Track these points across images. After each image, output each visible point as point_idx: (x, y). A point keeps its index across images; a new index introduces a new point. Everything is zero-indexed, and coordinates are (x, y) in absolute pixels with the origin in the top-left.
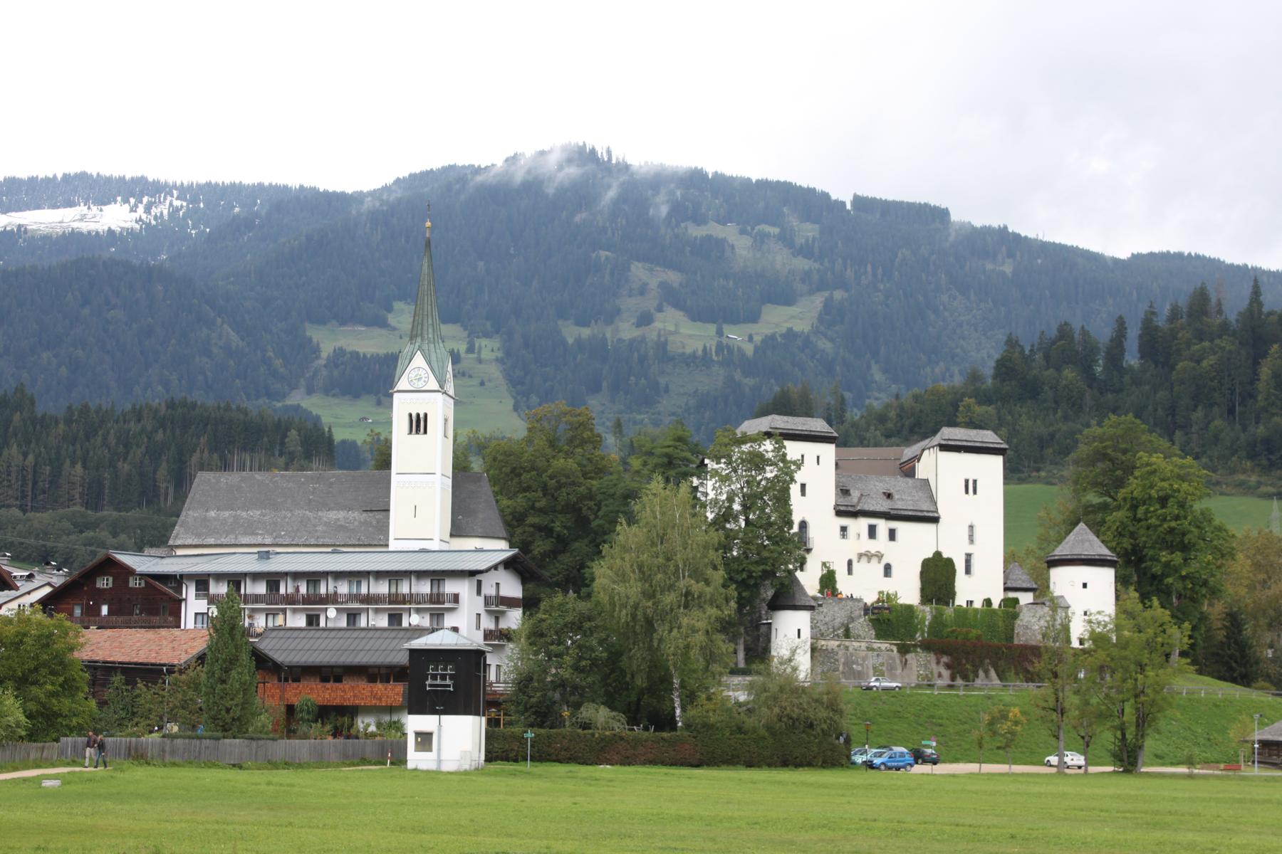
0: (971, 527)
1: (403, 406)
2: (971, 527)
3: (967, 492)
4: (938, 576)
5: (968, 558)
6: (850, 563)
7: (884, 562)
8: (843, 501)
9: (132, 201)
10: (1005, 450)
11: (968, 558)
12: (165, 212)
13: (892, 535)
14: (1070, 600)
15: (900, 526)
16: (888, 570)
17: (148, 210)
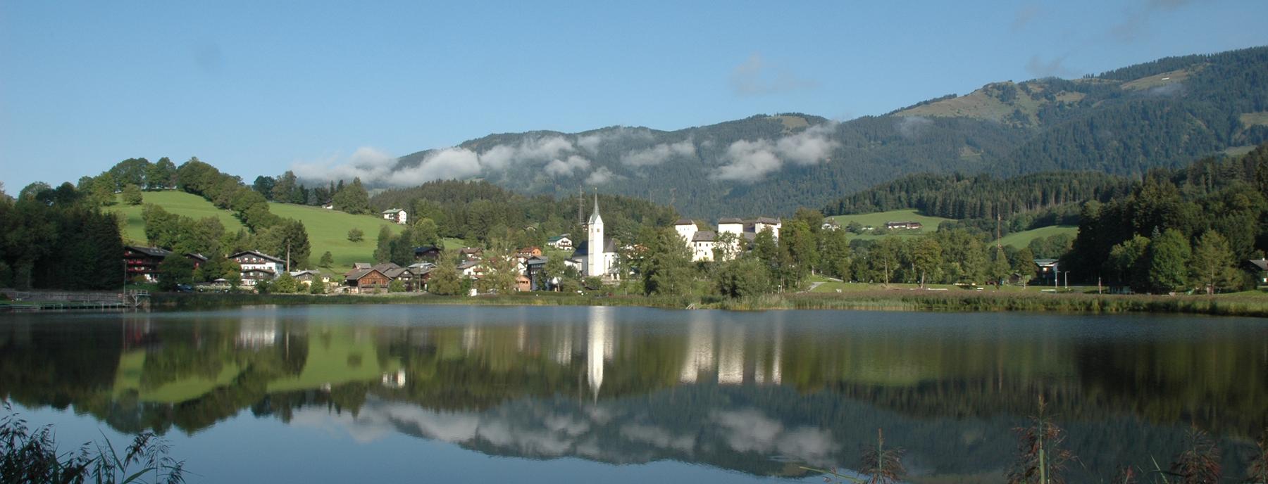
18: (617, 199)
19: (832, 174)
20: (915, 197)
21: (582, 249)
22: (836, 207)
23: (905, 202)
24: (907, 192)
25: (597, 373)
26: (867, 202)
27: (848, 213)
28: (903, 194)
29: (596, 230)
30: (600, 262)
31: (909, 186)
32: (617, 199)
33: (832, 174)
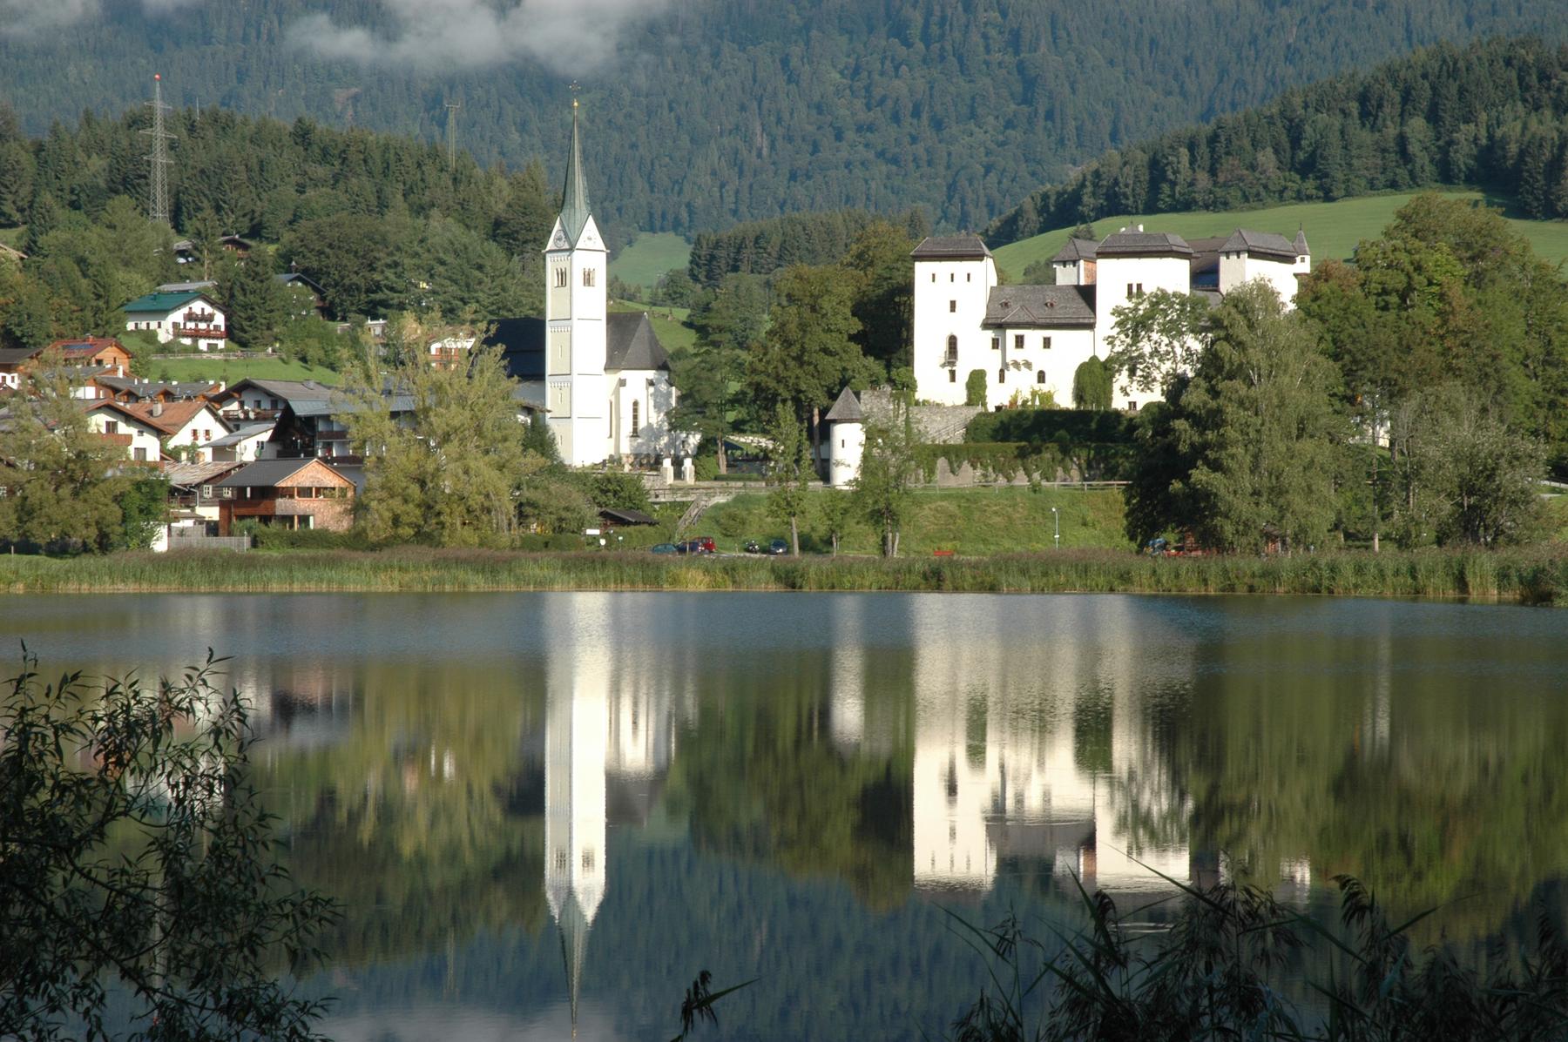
0: (953, 341)
2: (953, 341)
8: (1000, 312)
13: (1047, 343)
15: (1054, 334)
16: (1041, 377)
18: (303, 135)
19: (1015, 41)
20: (1466, 139)
21: (522, 346)
22: (1132, 179)
23: (1422, 159)
24: (1433, 117)
25: (579, 851)
26: (1267, 158)
27: (1186, 206)
28: (1417, 126)
29: (578, 288)
30: (599, 407)
31: (1440, 90)
32: (303, 135)
33: (1015, 41)
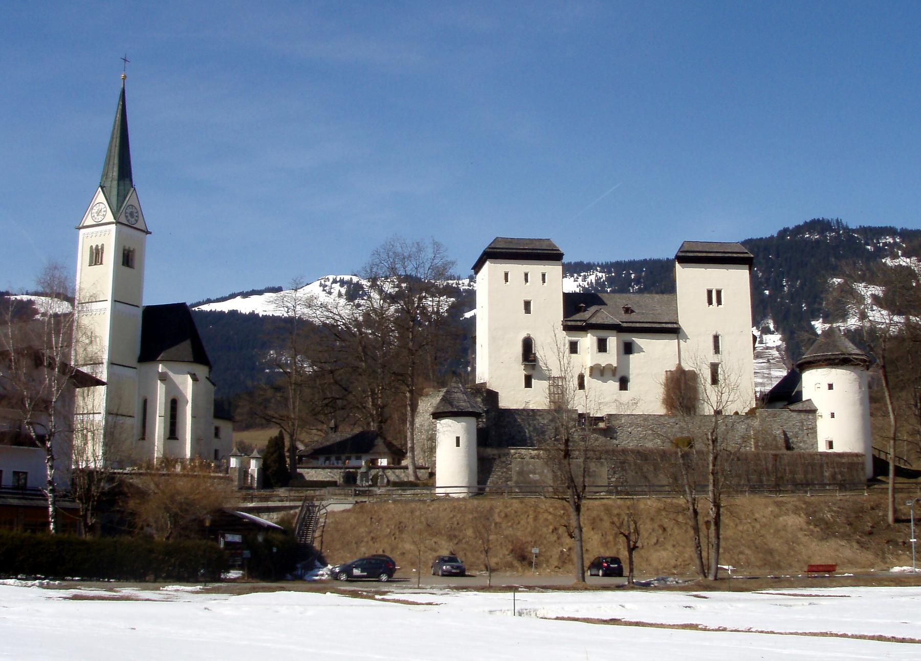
0: (716, 338)
1: (87, 240)
2: (716, 338)
3: (710, 302)
4: (682, 389)
5: (714, 368)
6: (581, 378)
7: (618, 376)
9: (576, 275)
10: (751, 259)
11: (714, 368)
12: (594, 281)
14: (817, 403)
17: (584, 280)
